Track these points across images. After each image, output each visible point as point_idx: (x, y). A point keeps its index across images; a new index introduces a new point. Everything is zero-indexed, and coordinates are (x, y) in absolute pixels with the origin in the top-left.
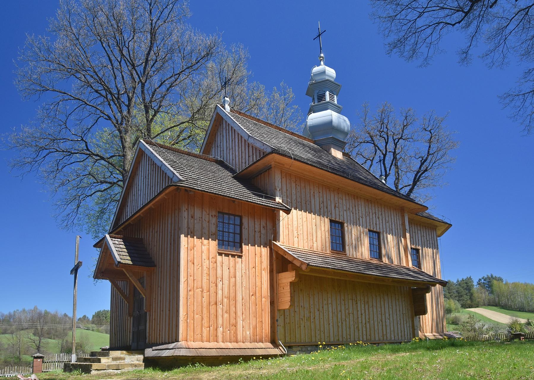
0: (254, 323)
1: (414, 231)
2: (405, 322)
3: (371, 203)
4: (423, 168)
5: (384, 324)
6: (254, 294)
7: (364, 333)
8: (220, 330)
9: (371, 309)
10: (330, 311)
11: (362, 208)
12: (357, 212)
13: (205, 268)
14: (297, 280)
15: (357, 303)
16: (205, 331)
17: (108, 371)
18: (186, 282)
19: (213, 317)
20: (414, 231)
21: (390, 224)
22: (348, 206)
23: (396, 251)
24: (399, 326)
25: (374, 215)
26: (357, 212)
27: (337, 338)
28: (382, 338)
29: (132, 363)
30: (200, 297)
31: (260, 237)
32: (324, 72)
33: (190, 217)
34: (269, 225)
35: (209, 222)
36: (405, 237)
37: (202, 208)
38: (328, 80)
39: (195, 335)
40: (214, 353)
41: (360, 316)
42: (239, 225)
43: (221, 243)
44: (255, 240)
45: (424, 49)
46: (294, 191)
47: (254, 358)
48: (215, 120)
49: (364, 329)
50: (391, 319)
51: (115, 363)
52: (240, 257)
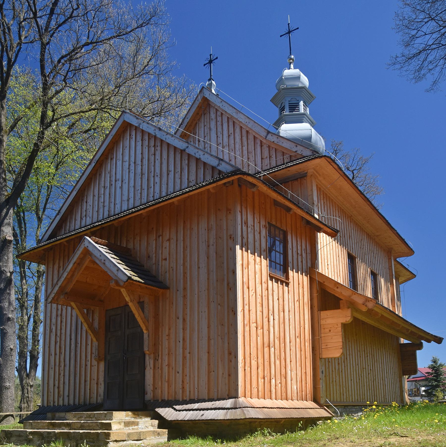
17: (128, 442)
32: (298, 78)
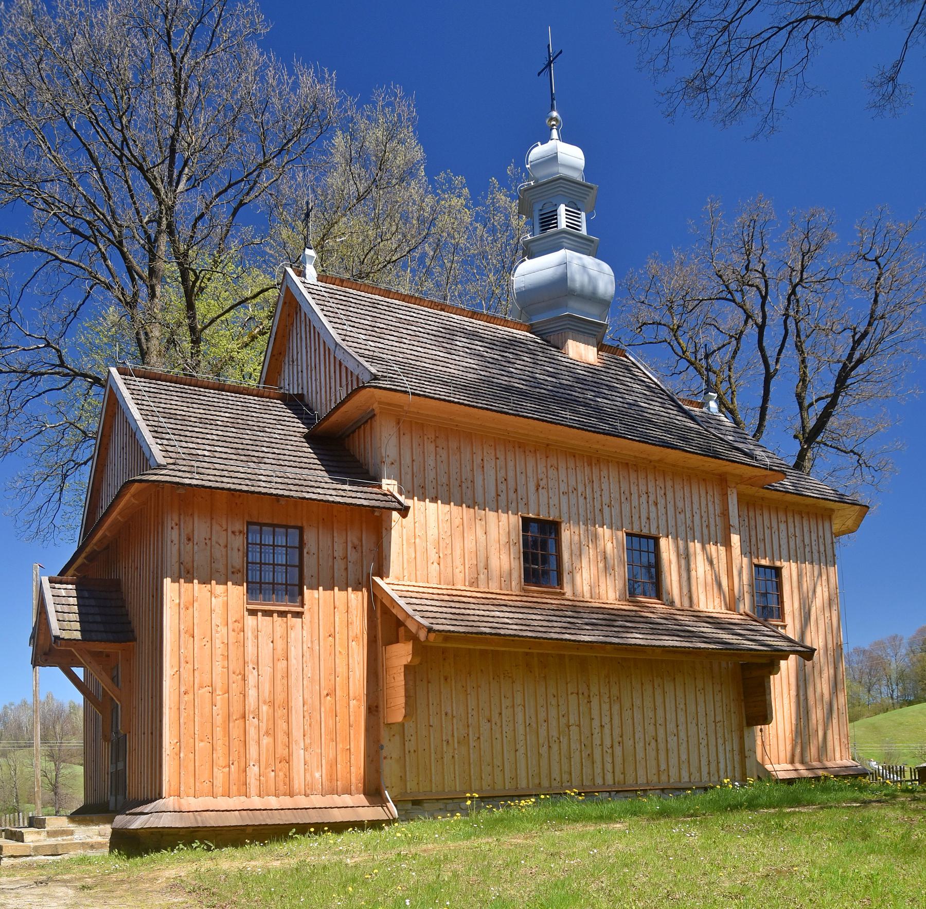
0: (332, 755)
1: (767, 523)
2: (720, 741)
3: (636, 471)
4: (857, 356)
5: (662, 746)
6: (331, 693)
7: (609, 767)
8: (253, 771)
9: (627, 714)
10: (514, 723)
11: (610, 484)
12: (597, 495)
13: (218, 643)
14: (417, 661)
15: (589, 702)
16: (219, 775)
17: (34, 858)
18: (177, 676)
19: (236, 745)
20: (767, 523)
21: (688, 515)
22: (572, 482)
23: (706, 580)
24: (704, 751)
25: (644, 499)
26: (597, 495)
27: (537, 782)
28: (655, 779)
29: (89, 840)
30: (208, 706)
31: (346, 569)
32: (553, 159)
33: (184, 538)
34: (368, 542)
35: (226, 546)
36: (727, 544)
37: (212, 519)
38: (560, 178)
39: (197, 784)
40: (233, 820)
41: (596, 731)
42: (281, 551)
43: (255, 589)
44: (333, 577)
45: (764, 87)
46: (431, 462)
47: (312, 830)
48: (285, 303)
49: (608, 759)
50: (682, 735)
51: (52, 841)
52: (299, 615)
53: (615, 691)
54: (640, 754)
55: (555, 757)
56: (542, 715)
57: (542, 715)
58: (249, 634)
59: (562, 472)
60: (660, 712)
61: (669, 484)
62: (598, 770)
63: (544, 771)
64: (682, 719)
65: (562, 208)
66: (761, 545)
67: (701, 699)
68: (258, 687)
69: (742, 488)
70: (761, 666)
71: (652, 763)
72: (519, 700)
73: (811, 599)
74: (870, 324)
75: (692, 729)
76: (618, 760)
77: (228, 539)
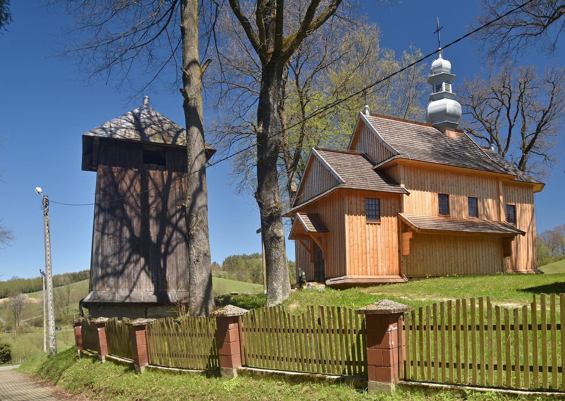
5: (478, 263)
7: (463, 269)
8: (369, 268)
9: (468, 253)
10: (438, 254)
11: (463, 182)
16: (360, 269)
22: (452, 182)
23: (492, 211)
24: (490, 265)
32: (441, 66)
40: (366, 281)
42: (377, 206)
43: (369, 217)
49: (462, 266)
50: (484, 259)
52: (379, 224)
53: (464, 246)
54: (472, 265)
55: (448, 266)
56: (444, 253)
57: (444, 253)
58: (367, 230)
59: (449, 179)
60: (478, 253)
61: (481, 180)
62: (460, 270)
63: (445, 269)
64: (484, 255)
65: (444, 84)
66: (509, 198)
67: (490, 248)
68: (370, 244)
69: (503, 180)
70: (509, 238)
71: (475, 268)
72: (437, 249)
73: (525, 217)
74: (550, 108)
75: (487, 257)
76: (465, 267)
77: (361, 203)
